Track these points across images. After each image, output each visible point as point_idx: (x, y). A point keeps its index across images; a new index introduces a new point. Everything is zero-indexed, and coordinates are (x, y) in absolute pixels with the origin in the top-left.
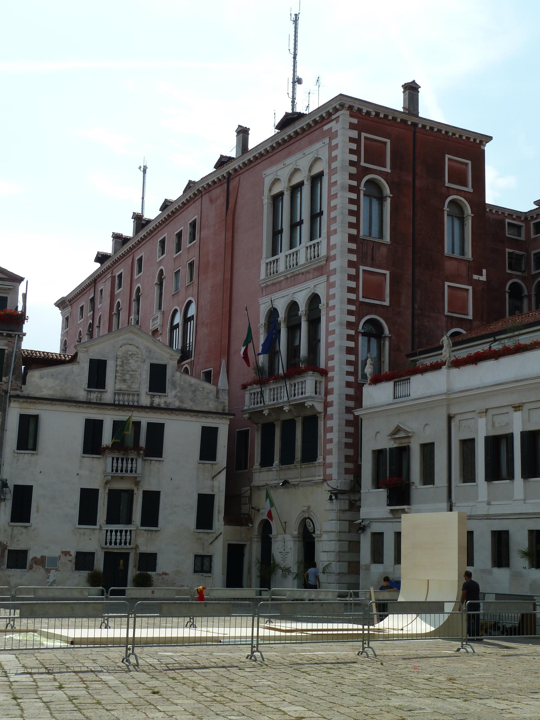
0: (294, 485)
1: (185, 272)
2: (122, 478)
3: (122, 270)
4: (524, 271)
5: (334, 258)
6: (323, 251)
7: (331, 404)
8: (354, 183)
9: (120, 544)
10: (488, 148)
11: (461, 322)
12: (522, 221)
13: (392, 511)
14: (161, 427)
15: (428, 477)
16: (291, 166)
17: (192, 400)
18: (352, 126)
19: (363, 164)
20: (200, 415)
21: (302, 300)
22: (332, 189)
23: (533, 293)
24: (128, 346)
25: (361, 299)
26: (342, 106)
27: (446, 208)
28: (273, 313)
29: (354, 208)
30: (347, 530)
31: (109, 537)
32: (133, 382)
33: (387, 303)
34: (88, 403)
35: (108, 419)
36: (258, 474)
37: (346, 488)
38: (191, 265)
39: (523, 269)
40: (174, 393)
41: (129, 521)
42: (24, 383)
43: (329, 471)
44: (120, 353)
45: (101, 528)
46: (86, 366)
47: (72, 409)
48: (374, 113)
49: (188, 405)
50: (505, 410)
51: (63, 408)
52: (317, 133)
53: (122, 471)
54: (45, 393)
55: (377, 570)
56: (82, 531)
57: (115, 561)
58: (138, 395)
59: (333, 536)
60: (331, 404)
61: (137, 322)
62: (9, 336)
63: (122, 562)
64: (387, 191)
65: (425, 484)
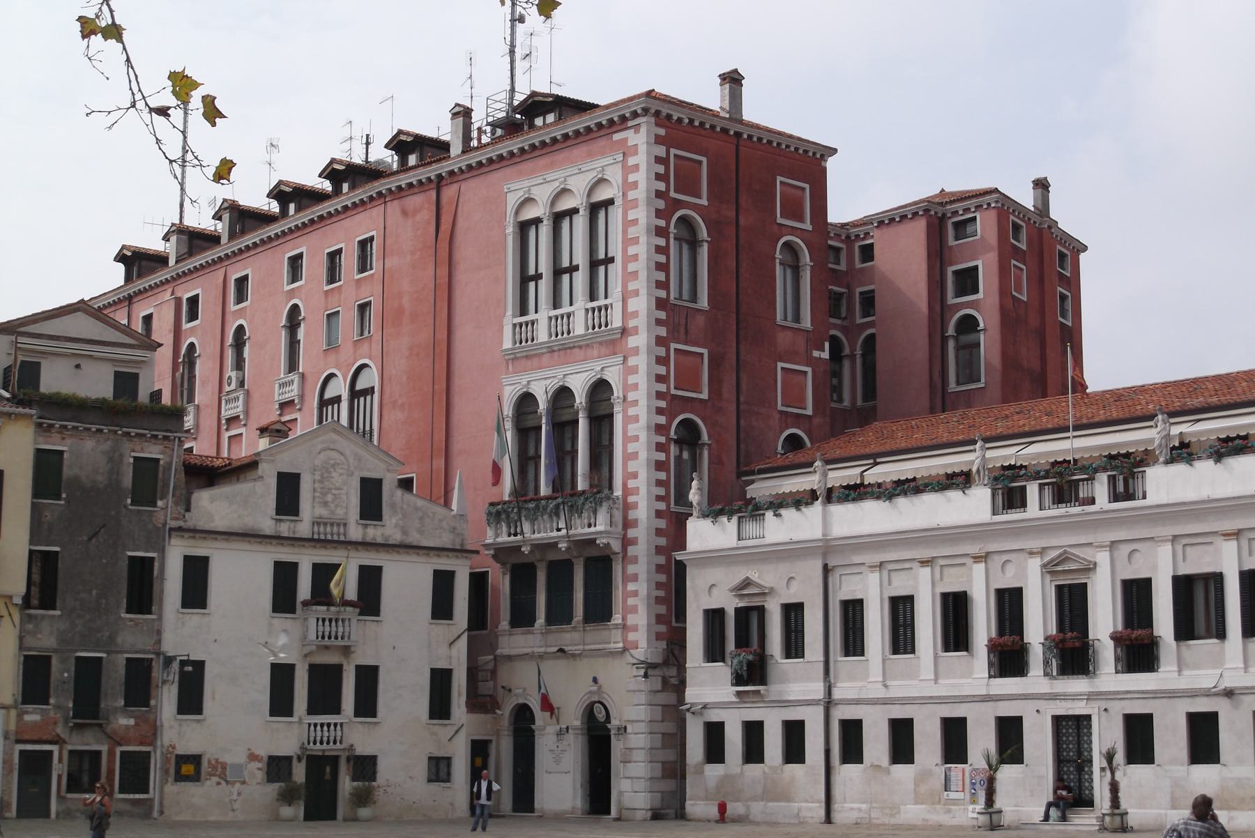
0: (573, 656)
1: (348, 318)
2: (327, 648)
3: (198, 291)
4: (845, 318)
5: (636, 331)
6: (617, 322)
7: (634, 542)
8: (662, 223)
9: (328, 743)
10: (831, 164)
11: (798, 420)
12: (842, 241)
13: (739, 694)
14: (205, 561)
15: (794, 647)
16: (556, 184)
17: (421, 532)
18: (659, 140)
19: (672, 194)
20: (432, 553)
21: (579, 385)
22: (630, 230)
23: (859, 352)
24: (329, 452)
25: (673, 391)
26: (646, 111)
27: (778, 255)
28: (526, 400)
29: (662, 259)
30: (660, 718)
31: (312, 734)
32: (337, 506)
33: (704, 395)
34: (278, 539)
35: (306, 562)
36: (506, 638)
37: (659, 660)
38: (363, 308)
39: (843, 315)
40: (394, 521)
41: (337, 710)
42: (188, 510)
43: (631, 636)
44: (317, 462)
45: (300, 721)
46: (273, 483)
47: (255, 547)
48: (687, 121)
49: (415, 538)
50: (907, 565)
51: (244, 545)
52: (602, 142)
53: (330, 637)
54: (220, 524)
55: (713, 771)
56: (275, 726)
57: (321, 767)
58: (345, 525)
59: (642, 727)
60: (634, 542)
61: (241, 384)
62: (166, 438)
63: (328, 769)
64: (703, 233)
65: (788, 656)
